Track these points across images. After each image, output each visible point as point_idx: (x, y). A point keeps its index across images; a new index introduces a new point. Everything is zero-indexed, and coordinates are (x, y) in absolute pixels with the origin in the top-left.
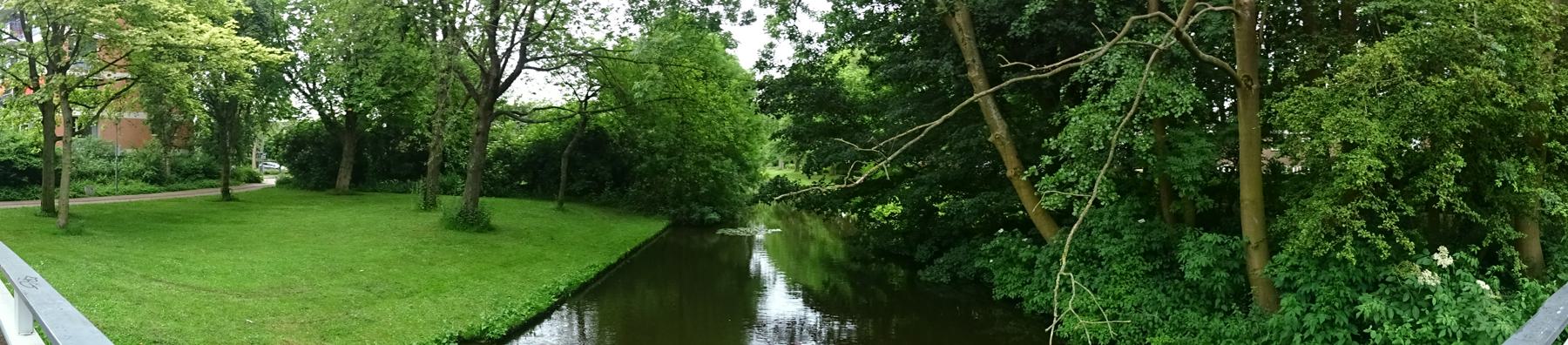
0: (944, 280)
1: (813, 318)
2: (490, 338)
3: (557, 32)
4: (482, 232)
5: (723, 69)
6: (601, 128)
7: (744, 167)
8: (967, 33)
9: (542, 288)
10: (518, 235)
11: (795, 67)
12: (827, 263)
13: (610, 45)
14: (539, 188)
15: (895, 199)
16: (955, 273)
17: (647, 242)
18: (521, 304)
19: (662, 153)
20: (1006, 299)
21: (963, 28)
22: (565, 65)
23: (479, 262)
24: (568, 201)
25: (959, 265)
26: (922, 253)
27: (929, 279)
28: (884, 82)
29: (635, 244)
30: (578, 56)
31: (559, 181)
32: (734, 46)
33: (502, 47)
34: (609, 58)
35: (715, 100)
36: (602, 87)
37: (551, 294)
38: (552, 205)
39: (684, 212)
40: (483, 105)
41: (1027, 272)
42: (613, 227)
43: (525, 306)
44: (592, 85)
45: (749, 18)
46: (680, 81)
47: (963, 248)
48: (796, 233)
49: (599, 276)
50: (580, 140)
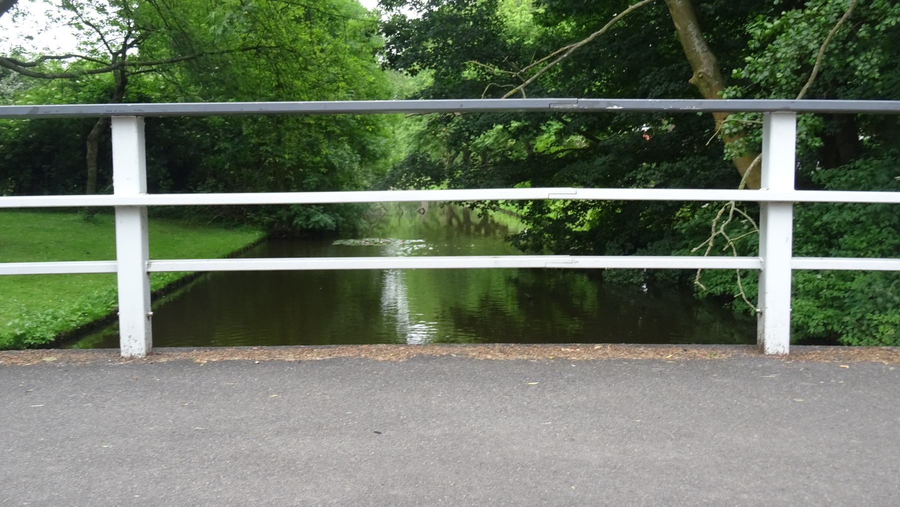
39: (284, 218)
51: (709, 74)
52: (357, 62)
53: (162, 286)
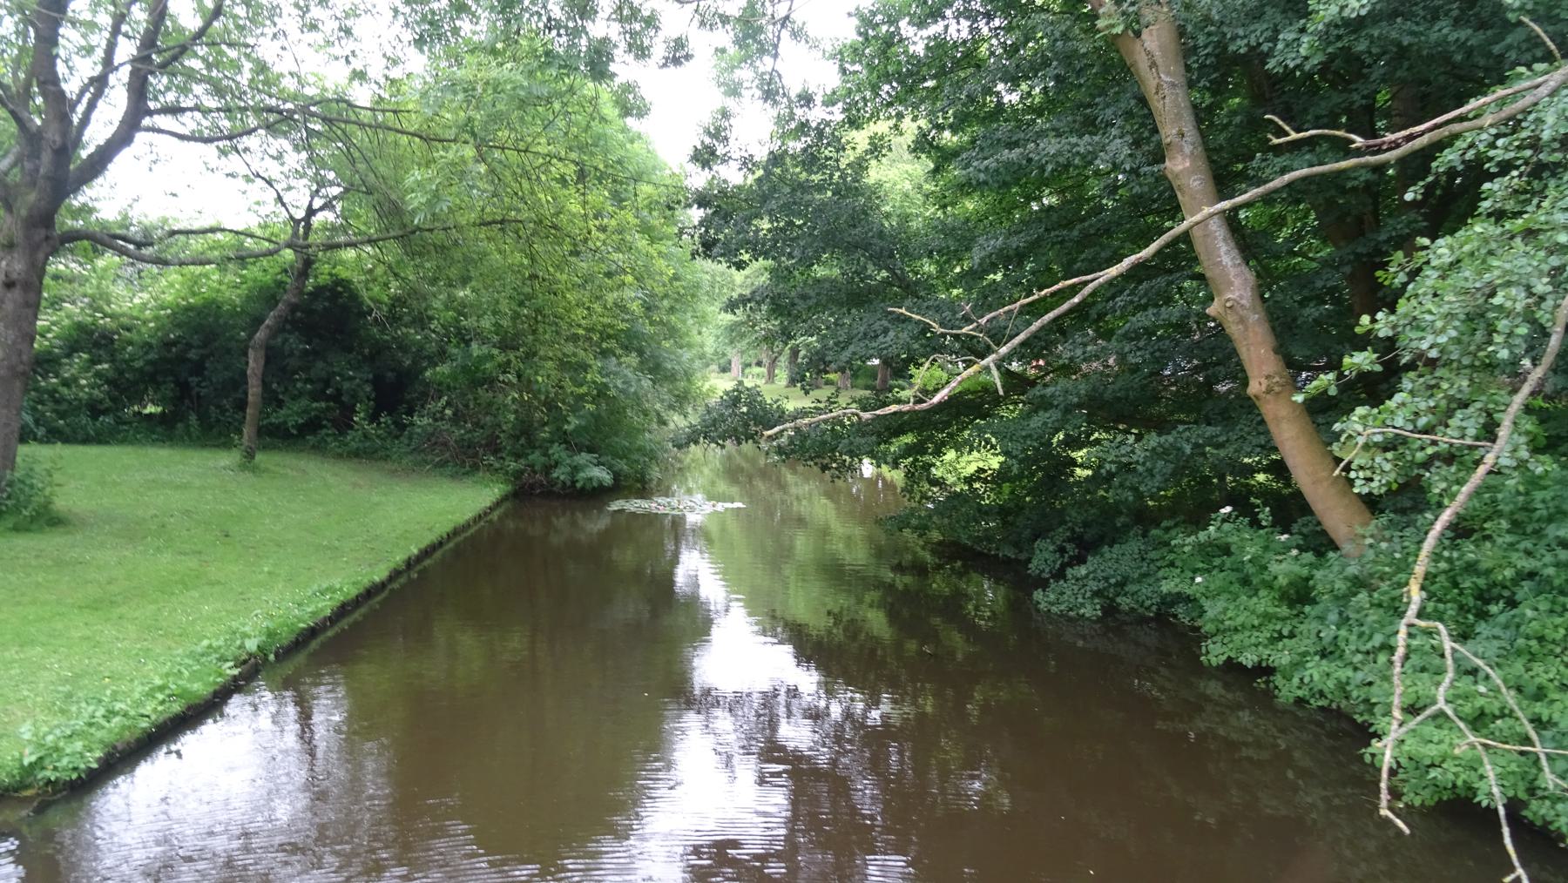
0: (1087, 611)
1: (807, 681)
2: (49, 782)
3: (232, 53)
4: (28, 530)
5: (619, 162)
6: (344, 283)
7: (654, 368)
8: (1168, 74)
9: (199, 649)
10: (131, 531)
11: (776, 159)
12: (835, 573)
13: (362, 96)
14: (193, 418)
15: (988, 442)
16: (1113, 600)
17: (456, 532)
18: (139, 690)
19: (484, 341)
20: (1231, 666)
21: (1159, 61)
22: (250, 132)
23: (19, 603)
24: (265, 448)
25: (1122, 584)
26: (1043, 557)
27: (1054, 609)
28: (966, 188)
29: (429, 538)
30: (287, 117)
31: (242, 405)
32: (641, 111)
33: (75, 74)
34: (361, 125)
35: (603, 229)
36: (346, 190)
37: (223, 659)
38: (226, 459)
40: (24, 212)
41: (1284, 611)
42: (377, 504)
43: (150, 694)
44: (322, 183)
45: (678, 54)
46: (526, 185)
47: (1133, 546)
48: (770, 513)
49: (343, 610)
50: (294, 308)
51: (1244, 302)
52: (646, 229)
53: (328, 612)
